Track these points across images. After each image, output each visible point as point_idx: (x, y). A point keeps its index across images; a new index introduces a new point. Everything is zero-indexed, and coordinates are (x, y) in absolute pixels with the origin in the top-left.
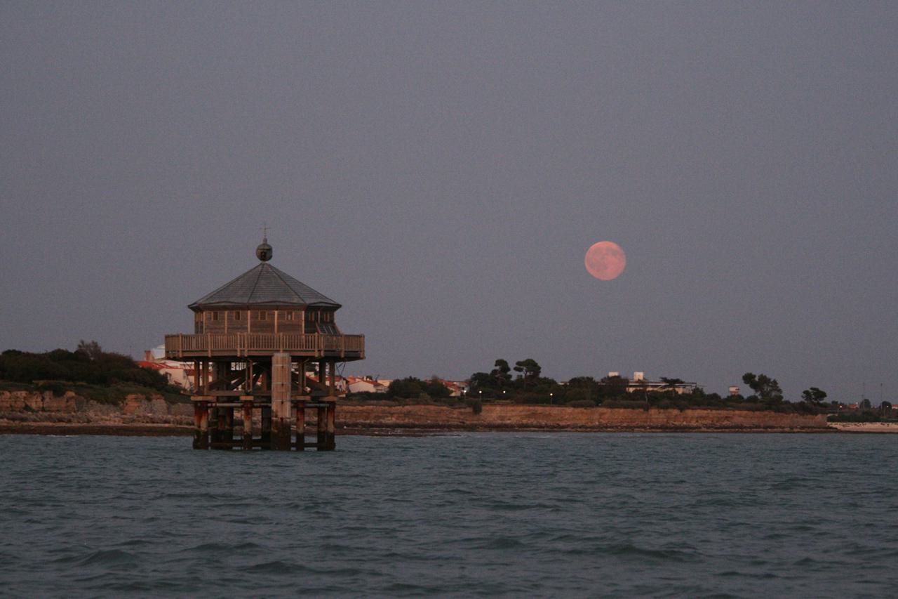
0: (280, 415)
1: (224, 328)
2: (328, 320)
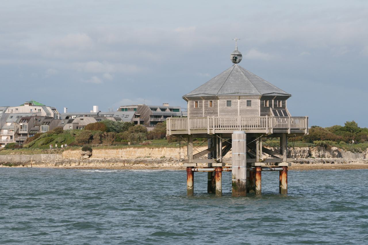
0: (237, 178)
1: (202, 113)
2: (281, 106)
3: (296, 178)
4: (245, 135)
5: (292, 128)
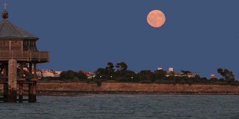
0: (12, 87)
2: (33, 45)
3: (50, 86)
4: (16, 61)
5: (41, 58)
